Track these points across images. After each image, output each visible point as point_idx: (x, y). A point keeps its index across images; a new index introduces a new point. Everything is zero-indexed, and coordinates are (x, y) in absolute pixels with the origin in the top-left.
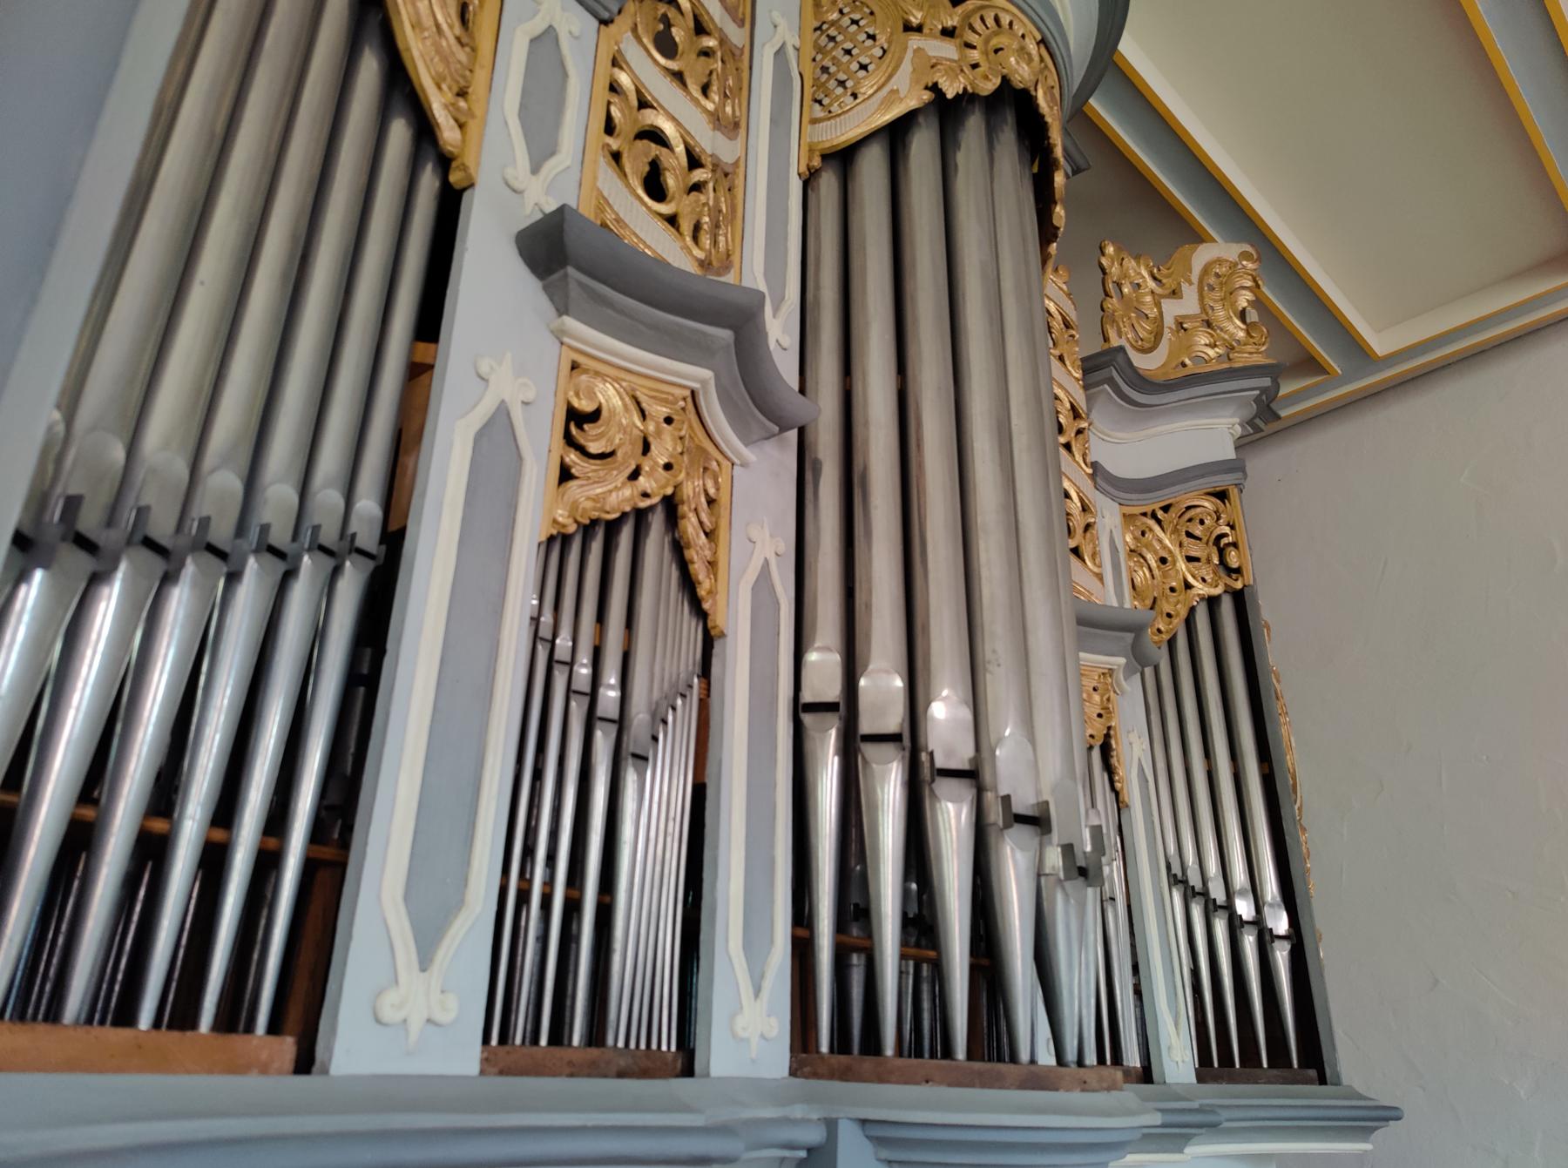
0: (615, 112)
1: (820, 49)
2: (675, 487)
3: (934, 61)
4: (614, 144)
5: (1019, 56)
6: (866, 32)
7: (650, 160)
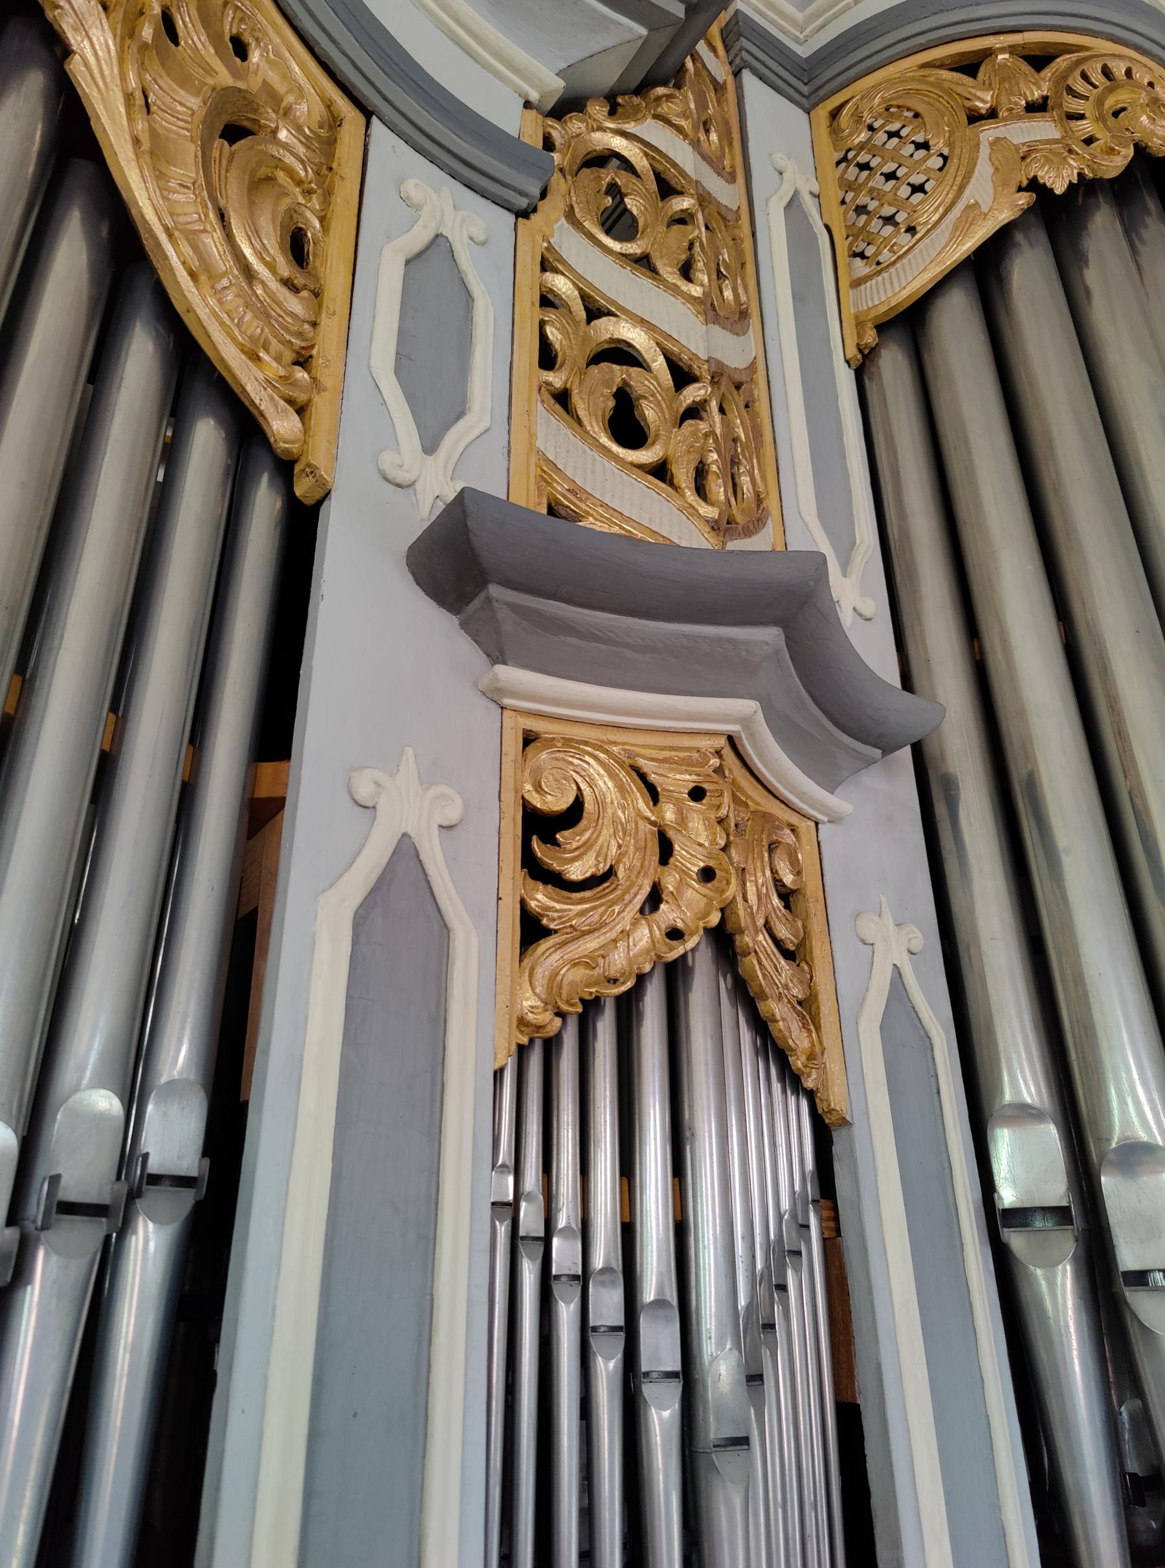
0: (552, 333)
1: (849, 186)
2: (722, 910)
3: (1025, 149)
4: (556, 379)
5: (1154, 112)
6: (913, 142)
7: (615, 390)
